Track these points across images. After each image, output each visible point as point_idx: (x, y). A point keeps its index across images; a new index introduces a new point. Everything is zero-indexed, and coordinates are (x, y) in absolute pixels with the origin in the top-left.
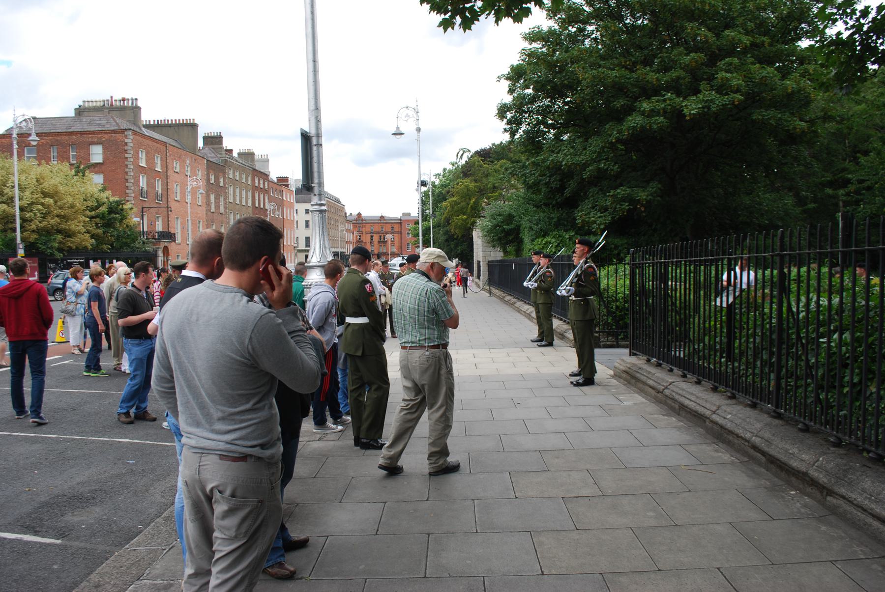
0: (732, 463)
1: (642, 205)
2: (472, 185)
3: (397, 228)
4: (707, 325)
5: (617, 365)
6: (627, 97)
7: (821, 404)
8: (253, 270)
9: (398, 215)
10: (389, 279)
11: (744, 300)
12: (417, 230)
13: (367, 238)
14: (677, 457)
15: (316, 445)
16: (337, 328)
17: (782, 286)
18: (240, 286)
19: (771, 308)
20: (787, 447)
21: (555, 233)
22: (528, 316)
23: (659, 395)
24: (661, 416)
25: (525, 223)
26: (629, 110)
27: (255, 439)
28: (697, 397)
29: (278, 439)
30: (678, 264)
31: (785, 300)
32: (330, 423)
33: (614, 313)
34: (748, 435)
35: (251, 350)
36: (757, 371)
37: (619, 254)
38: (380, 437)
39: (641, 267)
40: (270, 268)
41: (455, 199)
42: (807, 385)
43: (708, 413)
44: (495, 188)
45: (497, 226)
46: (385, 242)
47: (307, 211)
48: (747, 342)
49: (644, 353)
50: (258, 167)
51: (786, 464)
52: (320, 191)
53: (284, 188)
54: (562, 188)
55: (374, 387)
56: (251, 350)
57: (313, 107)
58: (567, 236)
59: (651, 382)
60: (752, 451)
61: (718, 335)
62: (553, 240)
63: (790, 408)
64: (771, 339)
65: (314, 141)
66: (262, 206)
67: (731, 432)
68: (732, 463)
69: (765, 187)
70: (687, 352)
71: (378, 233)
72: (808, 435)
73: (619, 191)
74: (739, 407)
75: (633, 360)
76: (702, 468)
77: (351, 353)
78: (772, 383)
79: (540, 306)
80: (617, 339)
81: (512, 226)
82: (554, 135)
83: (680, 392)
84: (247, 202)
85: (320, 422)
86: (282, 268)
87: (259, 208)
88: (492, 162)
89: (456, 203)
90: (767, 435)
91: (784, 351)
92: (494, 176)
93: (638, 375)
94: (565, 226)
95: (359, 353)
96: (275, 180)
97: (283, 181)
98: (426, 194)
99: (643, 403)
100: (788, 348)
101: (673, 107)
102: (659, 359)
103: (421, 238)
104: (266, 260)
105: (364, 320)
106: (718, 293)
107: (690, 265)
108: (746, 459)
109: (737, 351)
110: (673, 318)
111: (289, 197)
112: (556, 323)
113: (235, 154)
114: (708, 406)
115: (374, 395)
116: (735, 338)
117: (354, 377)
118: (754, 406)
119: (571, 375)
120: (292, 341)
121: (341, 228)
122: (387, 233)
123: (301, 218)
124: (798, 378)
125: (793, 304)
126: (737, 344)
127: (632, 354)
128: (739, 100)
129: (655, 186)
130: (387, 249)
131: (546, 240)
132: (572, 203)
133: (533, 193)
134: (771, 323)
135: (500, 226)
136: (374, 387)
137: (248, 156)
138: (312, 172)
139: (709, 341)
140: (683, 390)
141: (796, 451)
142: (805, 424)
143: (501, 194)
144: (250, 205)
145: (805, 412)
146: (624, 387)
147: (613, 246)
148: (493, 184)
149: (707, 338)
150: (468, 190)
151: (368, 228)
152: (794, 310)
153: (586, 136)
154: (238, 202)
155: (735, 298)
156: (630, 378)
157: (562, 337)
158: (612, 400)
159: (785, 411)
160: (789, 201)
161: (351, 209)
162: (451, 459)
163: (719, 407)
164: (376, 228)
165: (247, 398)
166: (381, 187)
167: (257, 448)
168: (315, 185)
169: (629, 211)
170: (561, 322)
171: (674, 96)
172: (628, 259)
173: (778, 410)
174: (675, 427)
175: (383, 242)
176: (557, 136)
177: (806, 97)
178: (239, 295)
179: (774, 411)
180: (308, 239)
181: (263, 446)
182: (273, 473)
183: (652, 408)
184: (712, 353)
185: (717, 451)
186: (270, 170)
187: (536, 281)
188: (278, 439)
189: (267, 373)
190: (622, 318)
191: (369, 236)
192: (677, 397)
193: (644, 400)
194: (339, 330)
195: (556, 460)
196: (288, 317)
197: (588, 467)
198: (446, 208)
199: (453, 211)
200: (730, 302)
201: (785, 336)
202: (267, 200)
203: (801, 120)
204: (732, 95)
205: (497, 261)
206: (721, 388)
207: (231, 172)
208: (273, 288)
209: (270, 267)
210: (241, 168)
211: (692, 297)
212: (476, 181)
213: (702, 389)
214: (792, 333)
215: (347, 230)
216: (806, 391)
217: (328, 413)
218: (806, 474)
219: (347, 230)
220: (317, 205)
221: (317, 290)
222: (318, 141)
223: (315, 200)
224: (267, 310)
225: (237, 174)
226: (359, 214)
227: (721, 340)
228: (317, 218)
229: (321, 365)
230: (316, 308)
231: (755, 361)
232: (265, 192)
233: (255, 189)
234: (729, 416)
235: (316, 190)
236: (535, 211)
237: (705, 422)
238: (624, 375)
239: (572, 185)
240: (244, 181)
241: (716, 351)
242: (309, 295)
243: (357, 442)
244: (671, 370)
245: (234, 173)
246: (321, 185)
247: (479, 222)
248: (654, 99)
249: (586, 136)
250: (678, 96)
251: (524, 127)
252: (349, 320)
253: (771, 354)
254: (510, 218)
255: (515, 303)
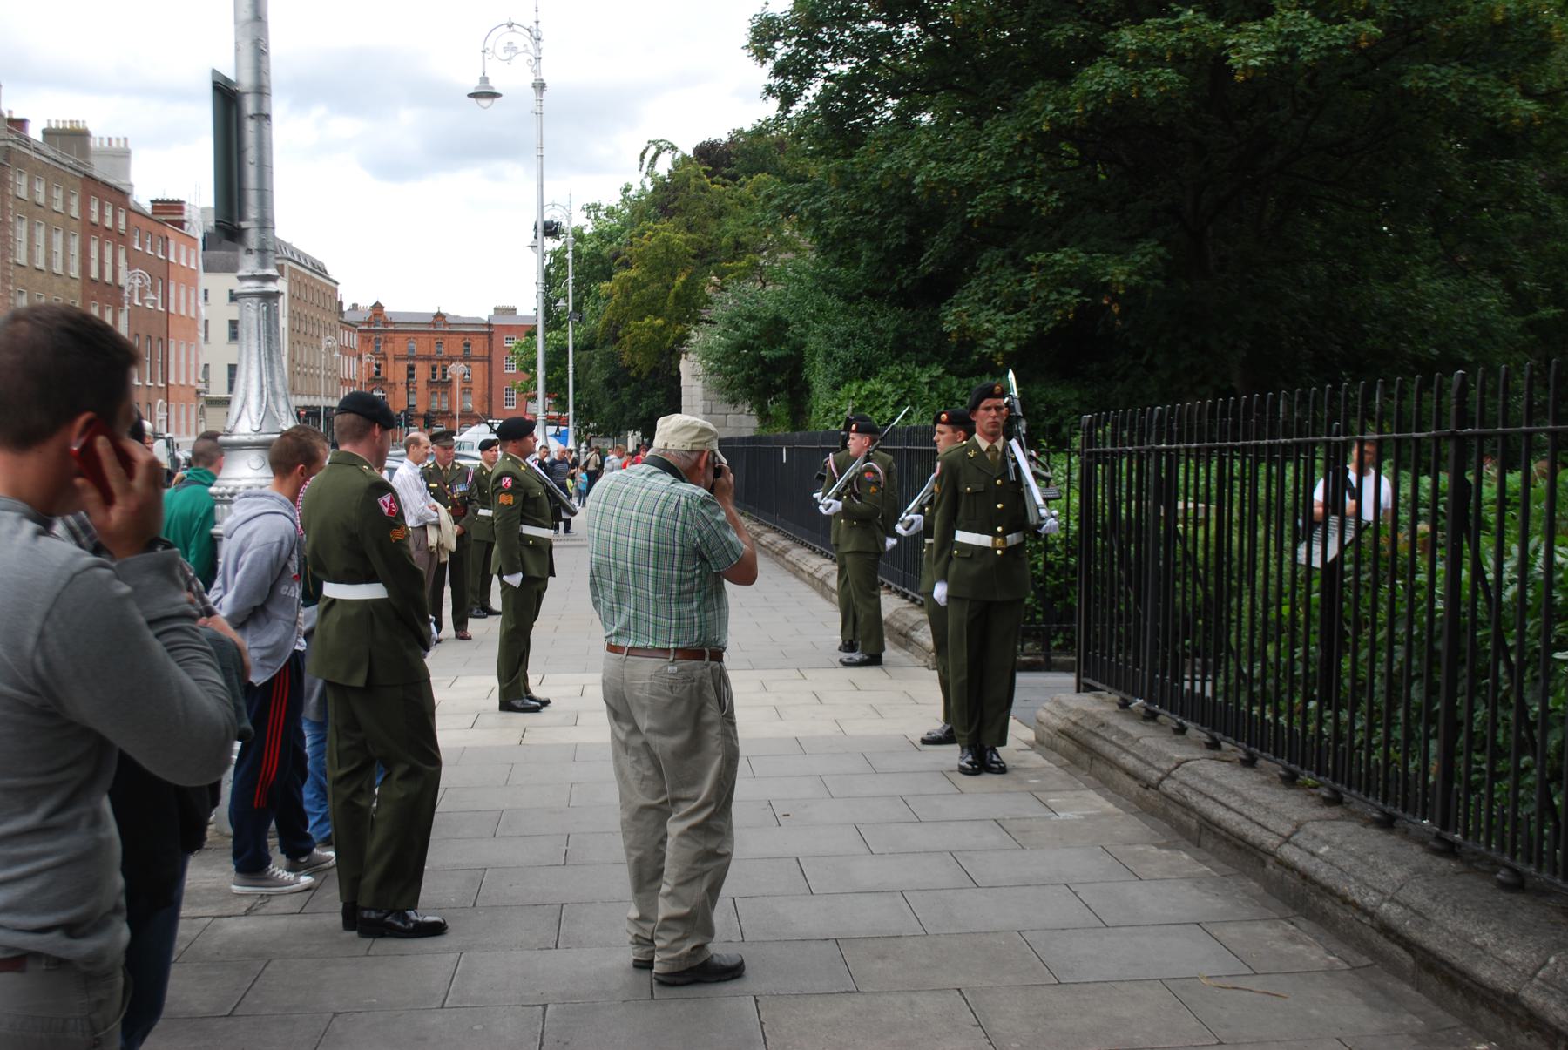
0: (1330, 971)
1: (1115, 298)
2: (679, 238)
3: (478, 347)
4: (1273, 614)
5: (1043, 715)
6: (1086, 17)
7: (1556, 819)
8: (51, 449)
9: (483, 312)
10: (453, 483)
11: (1367, 551)
12: (530, 350)
13: (397, 372)
14: (1192, 956)
15: (236, 927)
16: (304, 612)
17: (1462, 517)
18: (16, 493)
19: (1432, 574)
20: (1469, 928)
21: (892, 370)
22: (820, 586)
23: (1150, 794)
24: (1154, 850)
25: (813, 342)
26: (1092, 51)
27: (48, 909)
28: (1246, 800)
29: (116, 910)
30: (1202, 456)
31: (1467, 551)
32: (278, 868)
33: (1042, 579)
34: (1370, 899)
35: (41, 670)
36: (1398, 734)
37: (1056, 429)
38: (413, 904)
39: (1111, 460)
40: (102, 443)
41: (633, 273)
42: (1522, 772)
43: (1270, 841)
44: (739, 248)
45: (744, 345)
46: (447, 384)
47: (234, 297)
48: (1372, 659)
49: (1115, 685)
50: (99, 170)
51: (1464, 974)
52: (263, 242)
53: (170, 231)
54: (912, 252)
55: (400, 770)
56: (41, 670)
57: (247, 13)
58: (925, 379)
59: (1129, 761)
60: (1380, 941)
61: (1300, 639)
62: (889, 388)
63: (1478, 830)
64: (1432, 652)
65: (249, 106)
66: (108, 278)
67: (1327, 891)
68: (1330, 971)
69: (1431, 263)
70: (1221, 682)
71: (428, 358)
72: (1521, 899)
73: (1058, 256)
74: (1351, 827)
75: (1086, 702)
76: (1253, 983)
77: (338, 680)
78: (1434, 765)
79: (848, 559)
80: (1047, 647)
81: (782, 351)
82: (895, 112)
83: (1203, 786)
84: (66, 266)
85: (251, 864)
86: (135, 447)
87: (99, 283)
88: (734, 178)
89: (636, 285)
90: (1419, 898)
91: (1463, 685)
92: (737, 216)
93: (1097, 742)
94: (918, 350)
95: (359, 680)
96: (148, 208)
97: (169, 211)
98: (558, 256)
99: (1106, 815)
100: (1475, 676)
101: (1197, 44)
102: (1151, 700)
103: (541, 374)
104: (89, 423)
105: (372, 592)
106: (1304, 535)
107: (1232, 458)
108: (1366, 960)
109: (1347, 682)
110: (1188, 594)
111: (187, 257)
112: (890, 604)
113: (35, 133)
114: (1271, 822)
115: (399, 792)
116: (1343, 647)
117: (345, 744)
118: (1387, 823)
119: (924, 742)
120: (157, 644)
121: (327, 342)
122: (452, 359)
123: (218, 312)
124: (1497, 753)
125: (1490, 562)
126: (1346, 665)
127: (1081, 688)
128: (1370, 38)
129: (1147, 252)
130: (452, 402)
131: (868, 386)
132: (940, 288)
133: (839, 263)
134: (1431, 610)
135: (750, 348)
136: (400, 770)
137: (72, 138)
138: (242, 191)
139: (1278, 654)
140: (1210, 781)
141: (1489, 939)
142: (1514, 871)
143: (756, 264)
144: (75, 273)
145: (1514, 840)
146: (1062, 773)
147: (1042, 407)
148: (736, 237)
149: (1271, 649)
150: (669, 250)
151: (400, 346)
152: (1490, 576)
153: (979, 114)
154: (41, 264)
155: (1342, 547)
156: (1078, 751)
157: (905, 640)
158: (1031, 808)
159: (1465, 835)
160: (1492, 300)
161: (356, 293)
162: (720, 949)
163: (1298, 827)
164: (423, 346)
165: (28, 797)
166: (440, 240)
167: (53, 936)
168: (249, 224)
169: (1081, 309)
170: (904, 603)
171: (1202, 17)
172: (1077, 442)
173: (1448, 835)
174: (1188, 878)
175: (441, 383)
176: (903, 116)
177: (1541, 34)
178: (13, 515)
179: (1438, 837)
180: (233, 369)
181: (70, 929)
182: (100, 1003)
183: (1129, 826)
184: (1284, 686)
185: (1292, 939)
186: (133, 179)
187: (838, 497)
188: (116, 910)
189: (87, 732)
190: (1061, 593)
191: (402, 367)
192: (1194, 799)
193: (1110, 806)
194: (308, 617)
195: (879, 965)
196: (147, 580)
197: (960, 981)
198: (609, 297)
199: (622, 309)
200: (1330, 557)
201: (1466, 644)
202: (122, 263)
203: (1527, 93)
204: (1355, 24)
205: (742, 440)
206: (1307, 777)
207: (23, 181)
208: (108, 499)
209: (102, 443)
210: (52, 173)
211: (1235, 538)
212: (690, 229)
213: (1260, 778)
214: (1486, 638)
215: (344, 350)
216: (1517, 786)
217: (273, 842)
218: (1513, 999)
219: (344, 350)
220: (253, 277)
221: (252, 509)
222: (259, 104)
223: (249, 265)
224: (89, 558)
225: (40, 188)
226: (378, 307)
227: (1307, 651)
228: (253, 314)
229: (238, 709)
230: (246, 559)
231: (1391, 707)
232: (118, 238)
233: (91, 230)
234: (1324, 850)
235: (253, 238)
236: (844, 311)
237: (1264, 864)
238: (1063, 742)
239: (939, 245)
240: (58, 207)
241: (1293, 680)
242: (228, 520)
243: (353, 919)
244: (1181, 730)
245: (30, 185)
246: (265, 224)
247: (696, 336)
248: (1151, 22)
249: (979, 114)
250: (1214, 17)
251: (815, 88)
252: (331, 590)
253: (1432, 691)
254: (775, 328)
255: (758, 535)
